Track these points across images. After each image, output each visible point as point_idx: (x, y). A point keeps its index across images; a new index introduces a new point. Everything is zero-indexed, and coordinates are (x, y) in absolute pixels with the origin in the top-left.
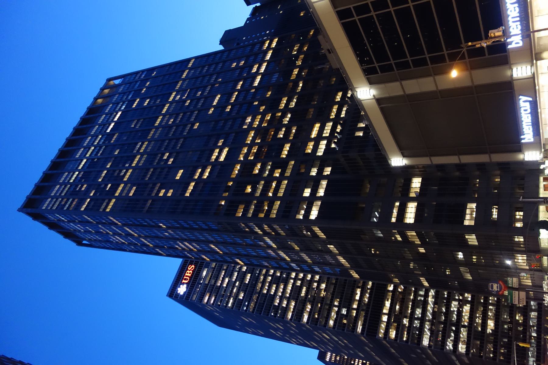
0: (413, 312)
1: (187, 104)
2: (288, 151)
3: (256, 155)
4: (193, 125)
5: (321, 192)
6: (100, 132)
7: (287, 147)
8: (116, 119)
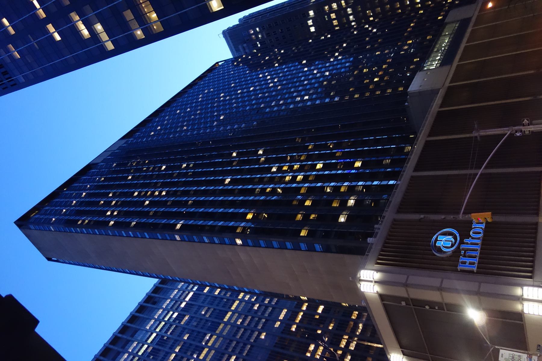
1: (256, 308)
4: (260, 334)
6: (171, 308)
8: (187, 299)
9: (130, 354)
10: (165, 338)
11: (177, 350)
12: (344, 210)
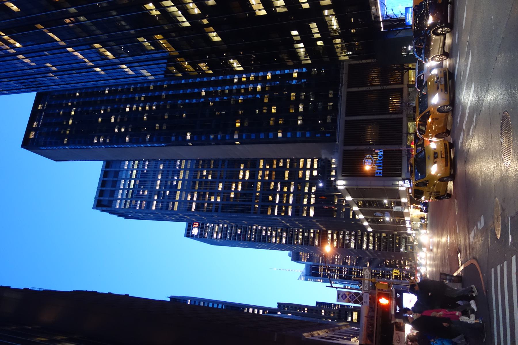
0: (177, 182)
2: (289, 175)
3: (270, 176)
5: (313, 201)
7: (287, 172)
9: (123, 189)
10: (142, 187)
11: (159, 177)
12: (235, 130)
